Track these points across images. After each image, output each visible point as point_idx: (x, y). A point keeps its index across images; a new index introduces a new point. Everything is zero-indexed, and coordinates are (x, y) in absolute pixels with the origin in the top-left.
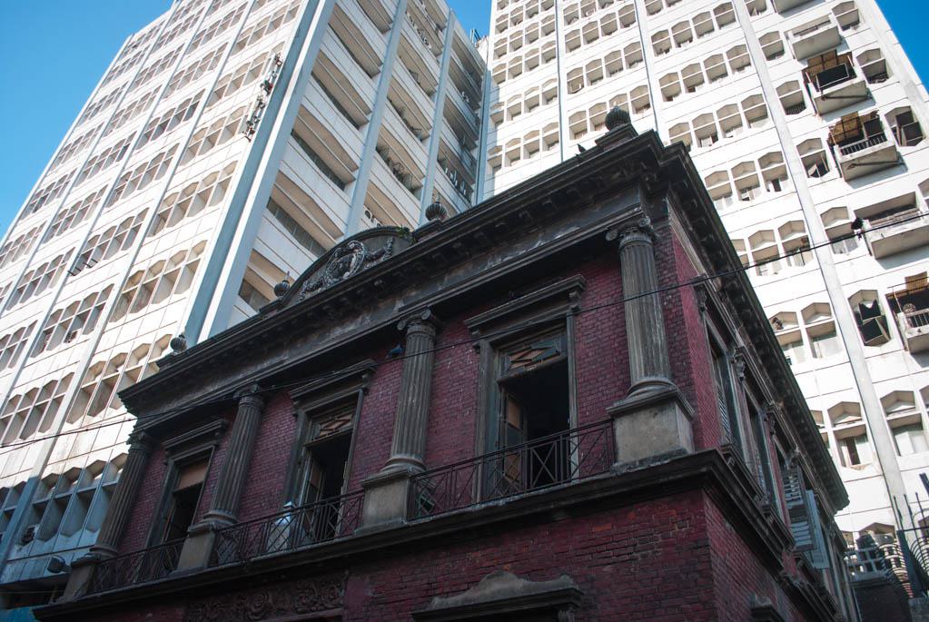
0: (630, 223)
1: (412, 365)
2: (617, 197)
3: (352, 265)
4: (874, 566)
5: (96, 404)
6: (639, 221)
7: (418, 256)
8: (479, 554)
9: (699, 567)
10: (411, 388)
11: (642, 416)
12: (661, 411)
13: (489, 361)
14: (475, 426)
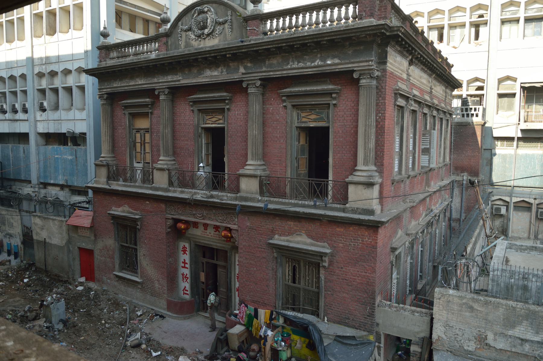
0: (366, 72)
2: (362, 48)
3: (208, 24)
4: (465, 115)
5: (48, 27)
7: (252, 49)
8: (292, 223)
10: (254, 125)
11: (360, 187)
12: (368, 188)
13: (291, 114)
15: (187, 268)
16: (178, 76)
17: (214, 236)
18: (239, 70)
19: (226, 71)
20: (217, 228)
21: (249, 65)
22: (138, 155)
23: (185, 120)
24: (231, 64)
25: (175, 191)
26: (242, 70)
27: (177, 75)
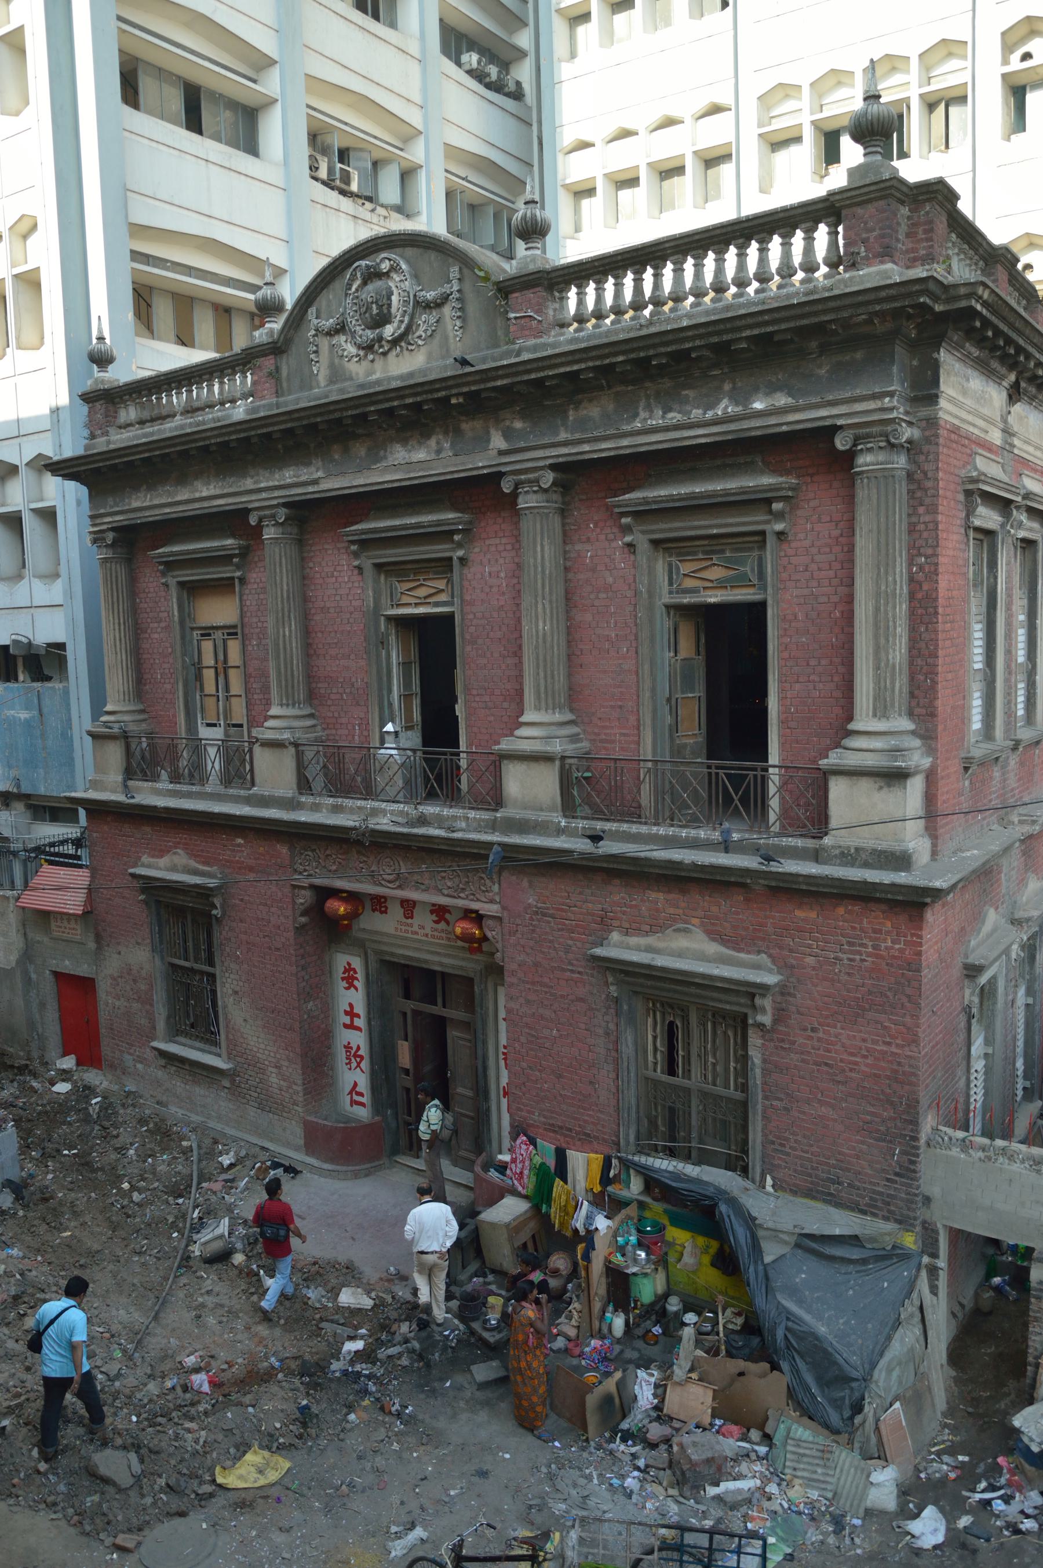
0: (875, 430)
1: (535, 567)
2: (859, 355)
3: (393, 310)
6: (889, 428)
7: (526, 377)
9: (908, 991)
10: (540, 606)
12: (889, 786)
15: (359, 1029)
16: (313, 469)
17: (433, 937)
18: (488, 441)
20: (440, 912)
21: (518, 425)
22: (210, 702)
23: (338, 598)
25: (316, 808)
26: (498, 442)
27: (308, 464)
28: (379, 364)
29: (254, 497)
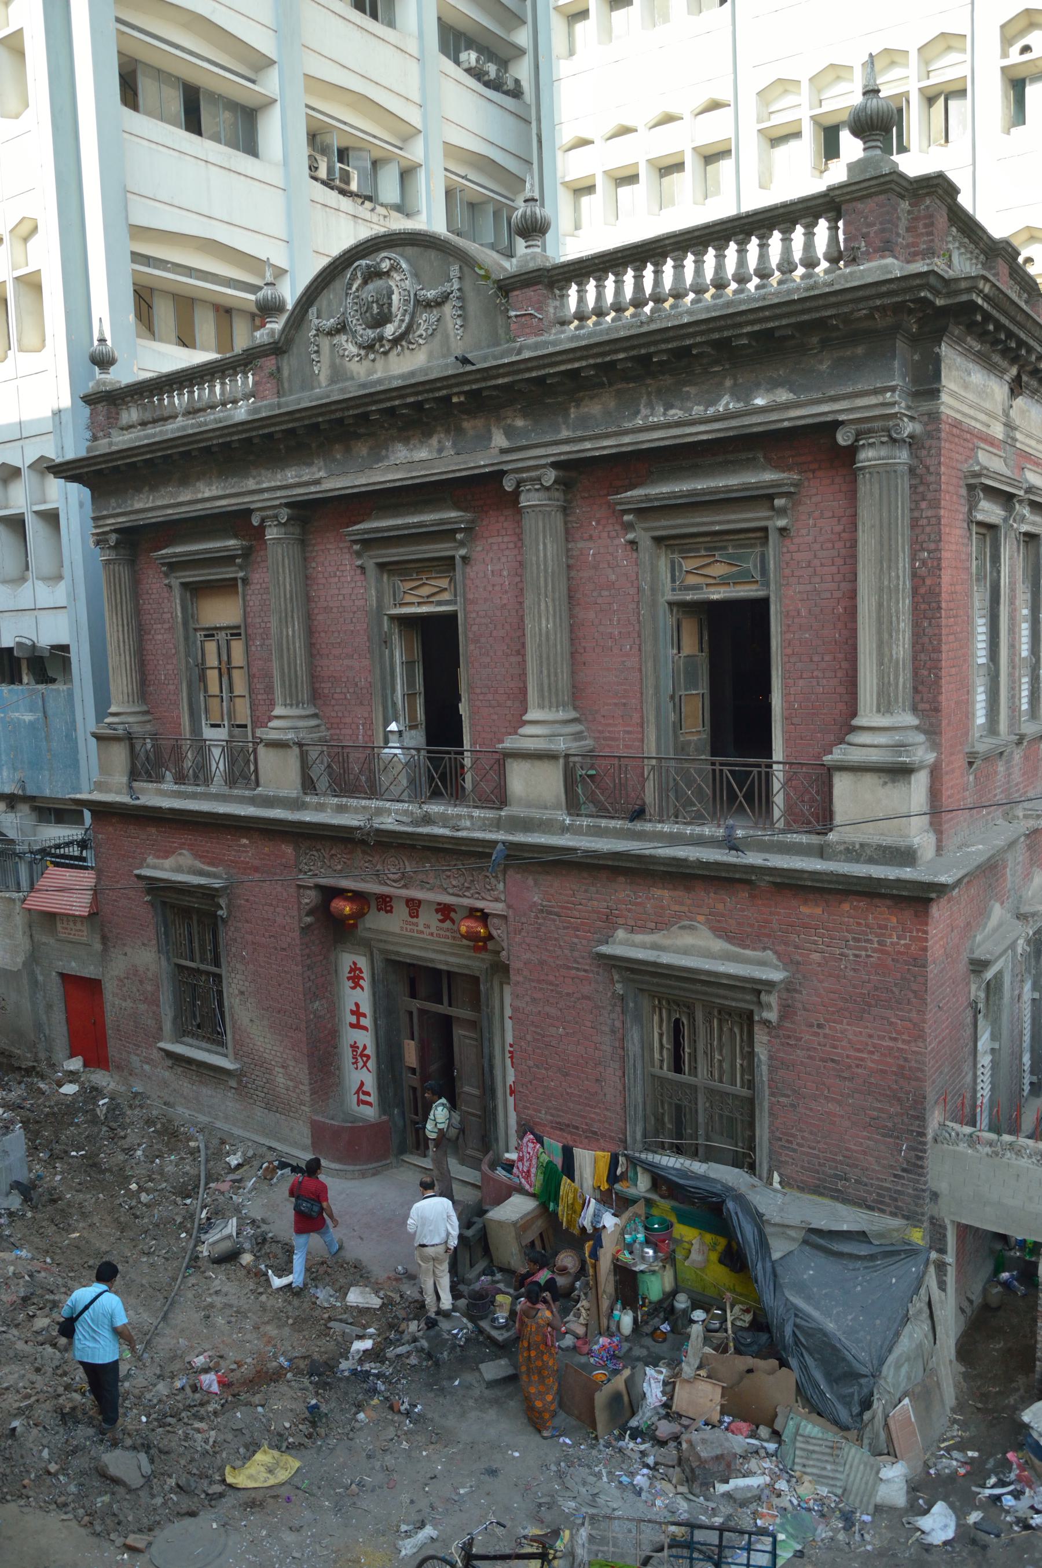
2: (860, 350)
3: (394, 309)
7: (527, 375)
8: (666, 893)
12: (894, 781)
14: (640, 670)
15: (365, 1028)
16: (315, 469)
17: (438, 935)
18: (490, 439)
19: (454, 445)
20: (445, 911)
21: (520, 423)
22: (214, 703)
24: (466, 425)
25: (320, 808)
26: (499, 440)
27: (310, 464)
28: (380, 364)
29: (256, 498)
